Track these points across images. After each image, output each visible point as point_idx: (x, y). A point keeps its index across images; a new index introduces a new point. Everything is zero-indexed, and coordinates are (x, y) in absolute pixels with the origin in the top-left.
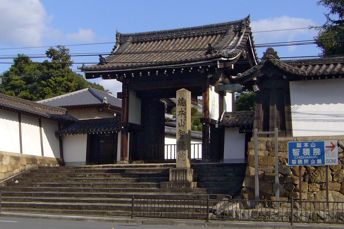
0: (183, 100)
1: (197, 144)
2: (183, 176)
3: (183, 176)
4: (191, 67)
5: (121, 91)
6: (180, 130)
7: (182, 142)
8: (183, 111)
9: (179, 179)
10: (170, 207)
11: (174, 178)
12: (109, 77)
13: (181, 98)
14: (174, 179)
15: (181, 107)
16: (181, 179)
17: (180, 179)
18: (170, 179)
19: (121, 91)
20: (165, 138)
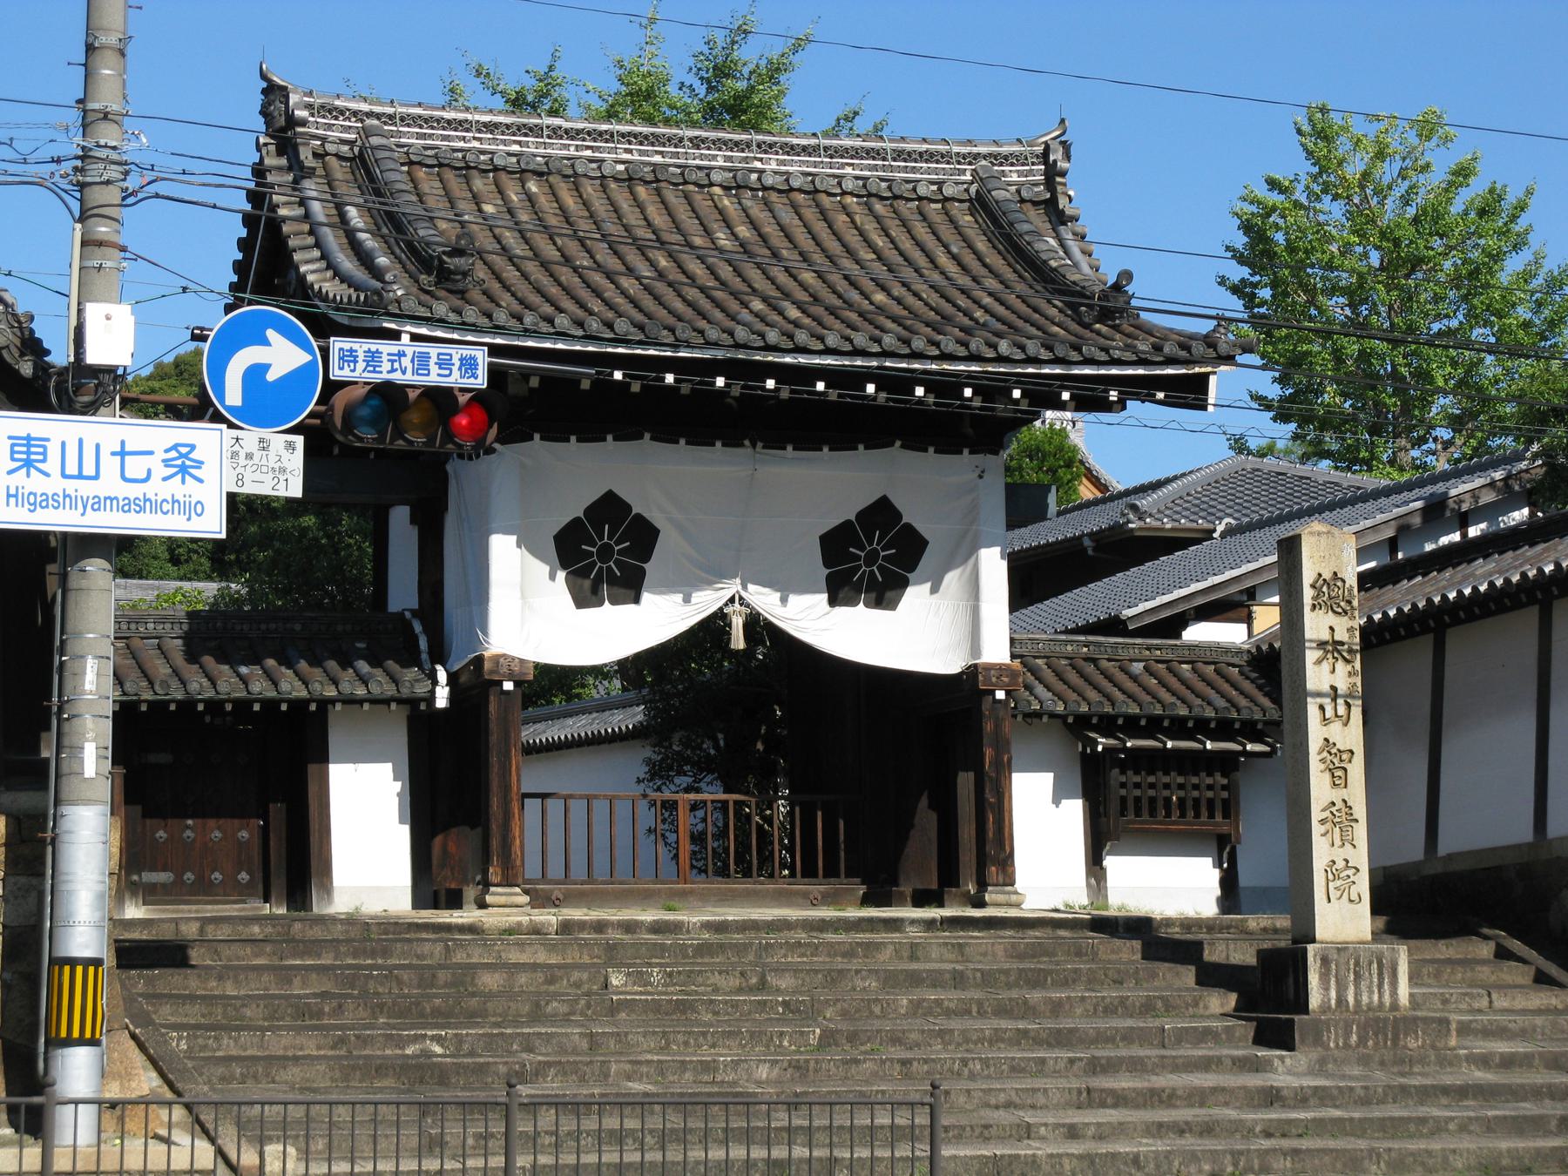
0: (1339, 584)
1: (581, 797)
2: (1380, 986)
3: (1380, 986)
4: (968, 385)
5: (514, 538)
6: (1326, 740)
7: (1340, 805)
8: (1342, 644)
9: (1358, 1001)
10: (357, 1169)
11: (1333, 994)
12: (1464, 535)
13: (1327, 575)
14: (1333, 1002)
15: (1331, 619)
16: (1371, 1002)
17: (1365, 999)
18: (1314, 1001)
19: (514, 538)
20: (1015, 776)
